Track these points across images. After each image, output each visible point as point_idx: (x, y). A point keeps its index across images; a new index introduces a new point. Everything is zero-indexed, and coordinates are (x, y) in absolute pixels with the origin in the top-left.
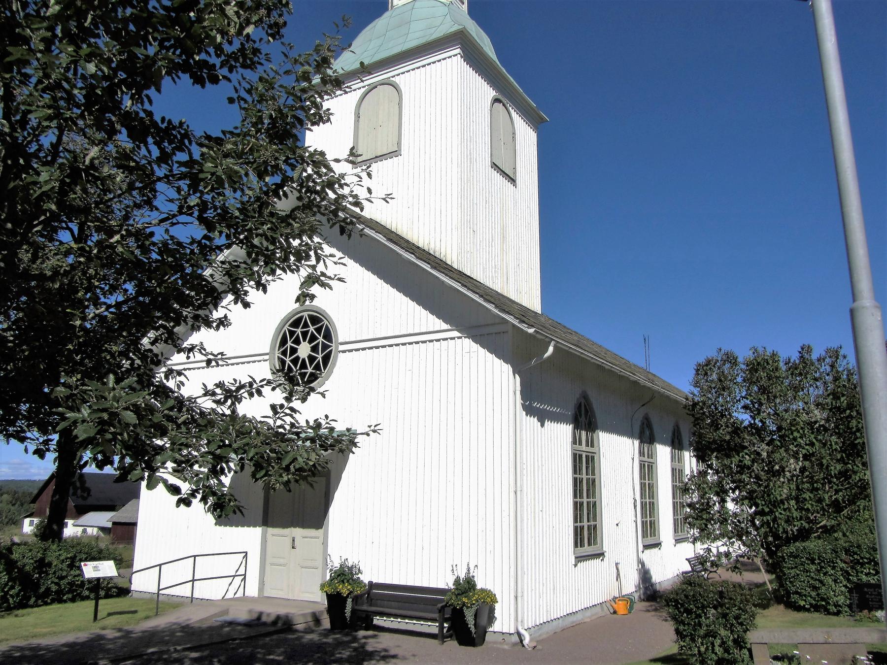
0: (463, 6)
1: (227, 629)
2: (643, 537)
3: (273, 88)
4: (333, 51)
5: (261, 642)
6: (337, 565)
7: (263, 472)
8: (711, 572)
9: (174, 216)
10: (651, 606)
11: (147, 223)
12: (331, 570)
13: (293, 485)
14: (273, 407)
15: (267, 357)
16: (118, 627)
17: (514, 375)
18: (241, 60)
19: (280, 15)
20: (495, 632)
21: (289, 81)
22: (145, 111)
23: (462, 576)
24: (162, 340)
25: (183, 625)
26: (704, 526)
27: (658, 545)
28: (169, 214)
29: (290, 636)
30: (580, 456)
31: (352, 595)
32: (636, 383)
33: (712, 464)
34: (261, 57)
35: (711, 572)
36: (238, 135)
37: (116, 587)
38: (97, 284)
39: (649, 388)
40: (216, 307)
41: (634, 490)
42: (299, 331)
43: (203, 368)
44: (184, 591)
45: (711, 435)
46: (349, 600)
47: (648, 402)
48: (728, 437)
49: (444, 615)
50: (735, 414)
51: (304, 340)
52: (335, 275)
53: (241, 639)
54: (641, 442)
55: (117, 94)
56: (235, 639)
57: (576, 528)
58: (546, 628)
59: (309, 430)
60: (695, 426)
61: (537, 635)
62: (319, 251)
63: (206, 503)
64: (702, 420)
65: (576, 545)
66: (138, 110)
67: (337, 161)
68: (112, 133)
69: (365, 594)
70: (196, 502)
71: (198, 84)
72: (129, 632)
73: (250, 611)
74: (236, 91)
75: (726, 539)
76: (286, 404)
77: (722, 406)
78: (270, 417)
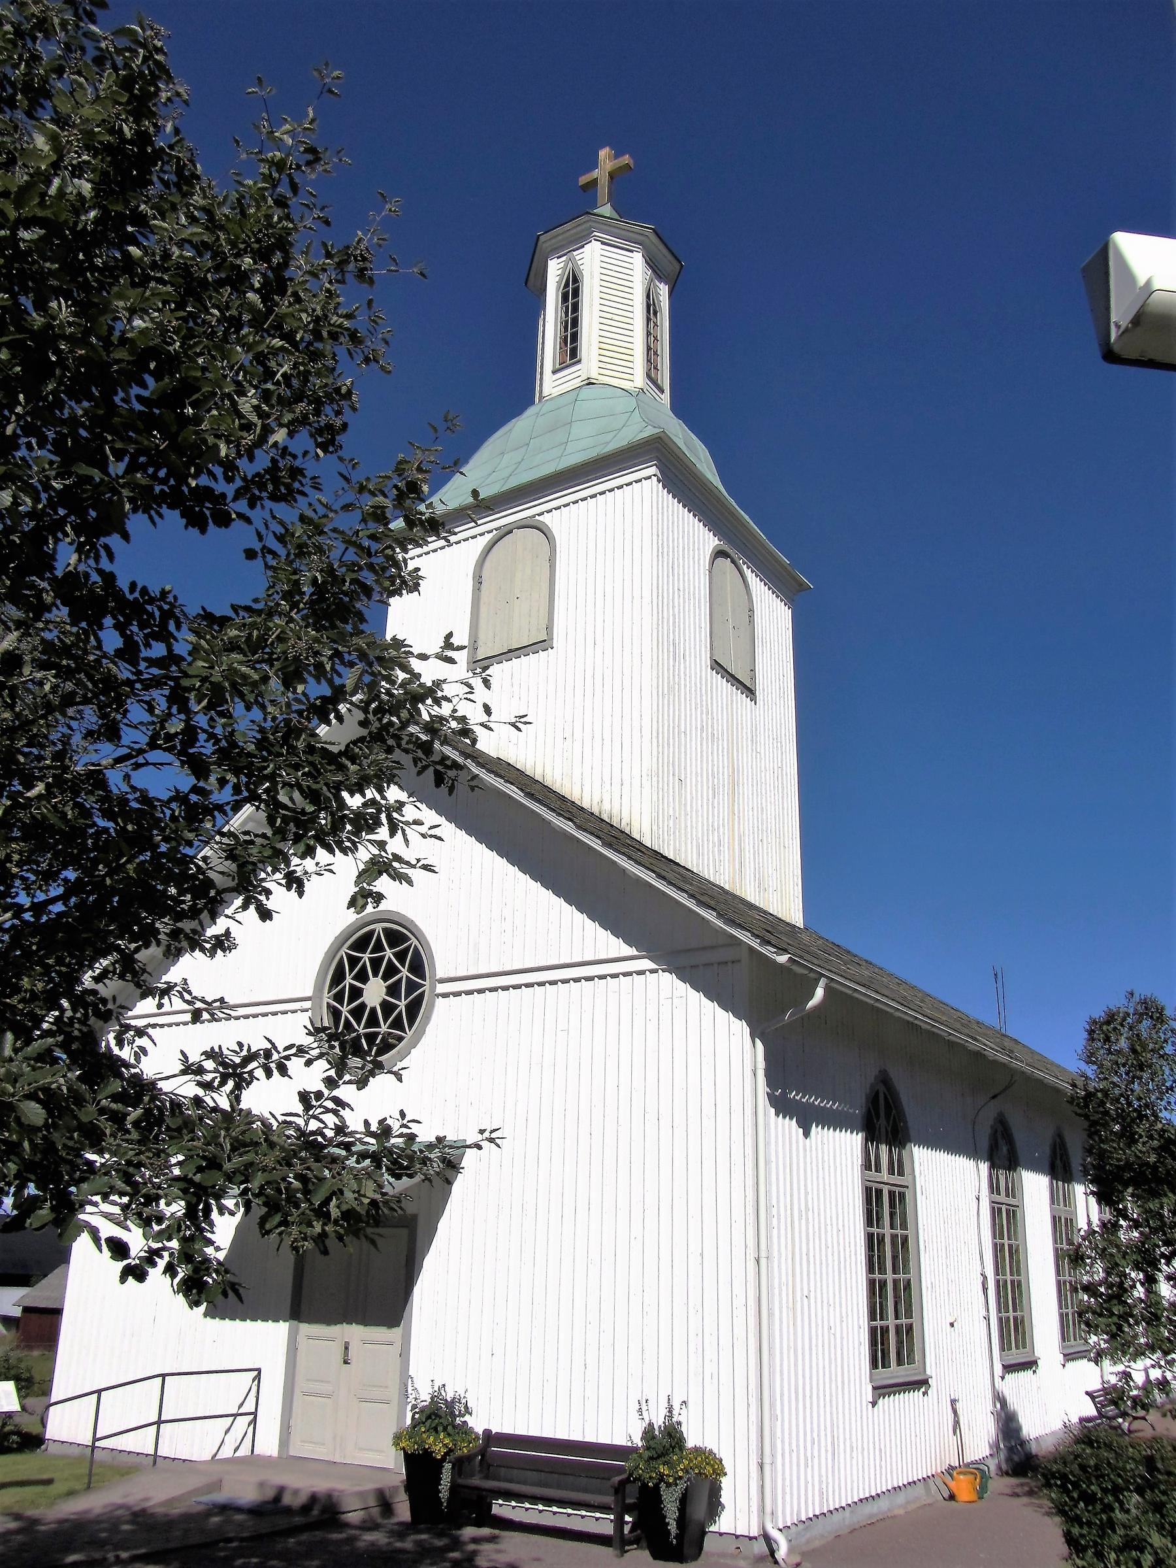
0: (662, 397)
1: (216, 1519)
2: (1002, 1349)
3: (322, 533)
4: (426, 472)
5: (279, 1547)
6: (425, 1396)
7: (277, 1218)
8: (1135, 1418)
9: (141, 752)
10: (1022, 1485)
11: (93, 764)
12: (414, 1407)
13: (332, 1243)
14: (304, 1097)
15: (308, 1004)
16: (16, 1509)
17: (754, 1042)
18: (270, 487)
19: (338, 413)
20: (721, 1534)
21: (349, 522)
22: (100, 572)
23: (659, 1421)
24: (114, 973)
25: (137, 1508)
26: (1114, 1328)
27: (1030, 1365)
28: (132, 749)
29: (335, 1536)
30: (879, 1193)
31: (452, 1457)
32: (979, 1056)
33: (1125, 1208)
34: (304, 481)
35: (1135, 1418)
36: (259, 612)
37: (18, 1433)
38: (15, 870)
39: (1004, 1065)
40: (214, 917)
41: (981, 1257)
42: (366, 957)
43: (186, 1024)
44: (141, 1442)
45: (1121, 1155)
46: (448, 1466)
47: (1004, 1090)
48: (1153, 1159)
49: (624, 1499)
50: (1164, 1114)
51: (375, 975)
52: (418, 860)
53: (242, 1540)
54: (993, 1166)
55: (47, 543)
56: (230, 1540)
57: (873, 1331)
58: (819, 1528)
59: (368, 1140)
60: (1090, 1136)
61: (803, 1540)
62: (395, 815)
63: (173, 1276)
64: (1102, 1125)
65: (874, 1364)
66: (88, 570)
67: (423, 657)
68: (40, 609)
69: (476, 1455)
70: (156, 1274)
71: (193, 527)
72: (35, 1522)
73: (262, 1485)
74: (260, 537)
75: (1159, 1354)
76: (326, 1092)
77: (1139, 1099)
78: (297, 1115)
